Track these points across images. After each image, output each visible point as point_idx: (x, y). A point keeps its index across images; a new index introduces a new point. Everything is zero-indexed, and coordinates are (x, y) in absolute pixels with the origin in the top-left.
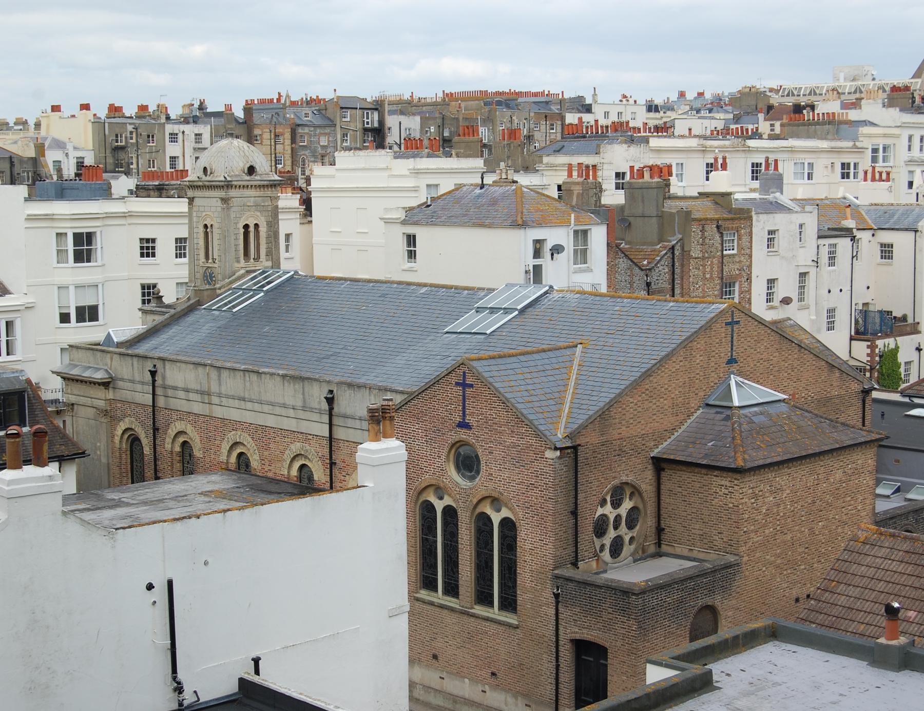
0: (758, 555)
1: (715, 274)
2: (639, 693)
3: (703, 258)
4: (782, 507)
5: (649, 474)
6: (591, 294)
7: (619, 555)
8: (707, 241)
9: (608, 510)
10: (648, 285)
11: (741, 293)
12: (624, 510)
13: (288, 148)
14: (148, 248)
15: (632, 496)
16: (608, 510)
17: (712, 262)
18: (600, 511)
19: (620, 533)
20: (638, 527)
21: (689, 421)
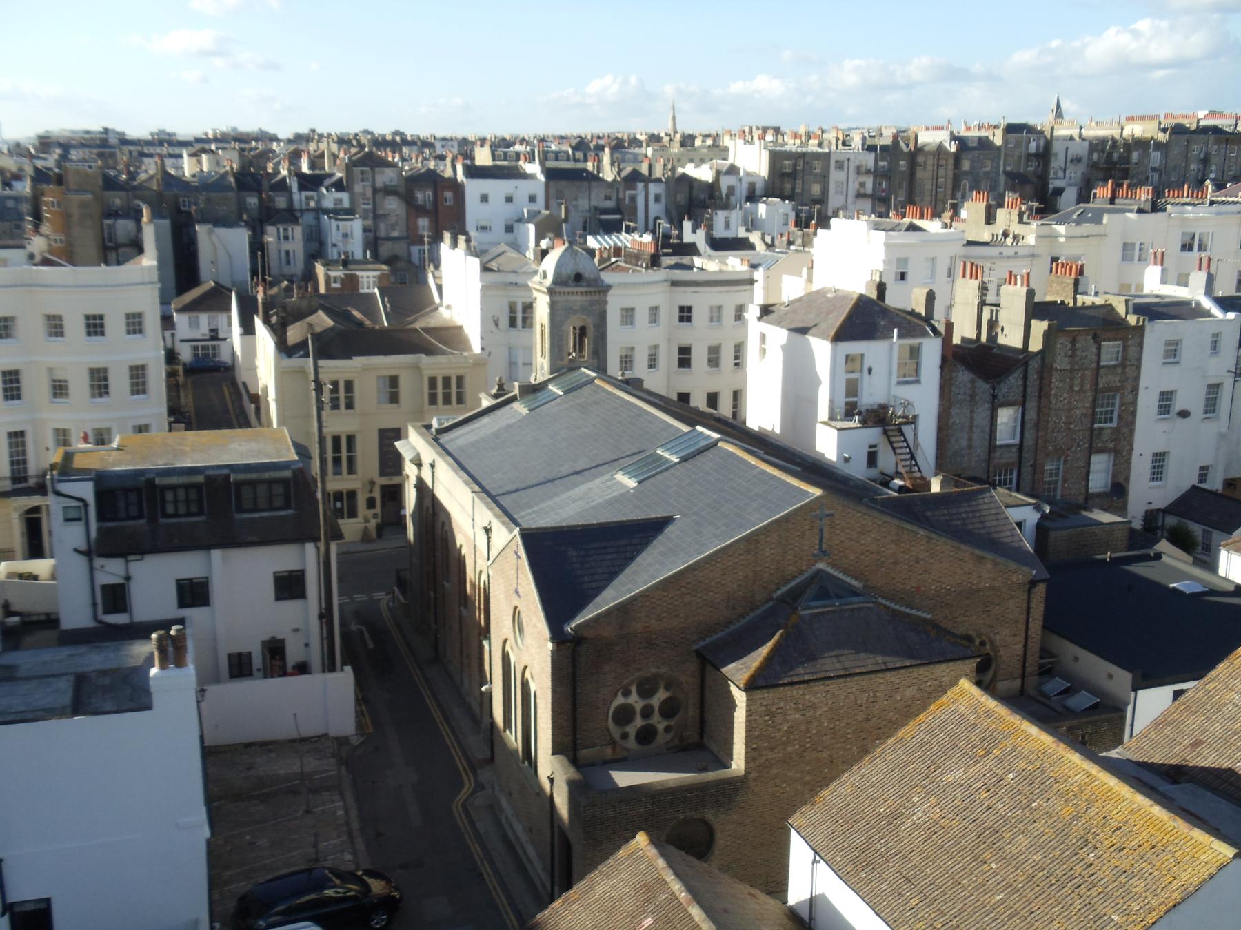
0: (774, 771)
1: (1088, 386)
2: (842, 790)
3: (1072, 371)
4: (815, 724)
5: (692, 666)
6: (759, 442)
7: (650, 742)
8: (1079, 353)
9: (634, 700)
10: (994, 397)
11: (1121, 405)
12: (656, 701)
13: (950, 173)
14: (12, 389)
15: (667, 688)
16: (634, 700)
17: (1083, 375)
18: (620, 700)
19: (651, 722)
20: (678, 717)
21: (752, 615)
